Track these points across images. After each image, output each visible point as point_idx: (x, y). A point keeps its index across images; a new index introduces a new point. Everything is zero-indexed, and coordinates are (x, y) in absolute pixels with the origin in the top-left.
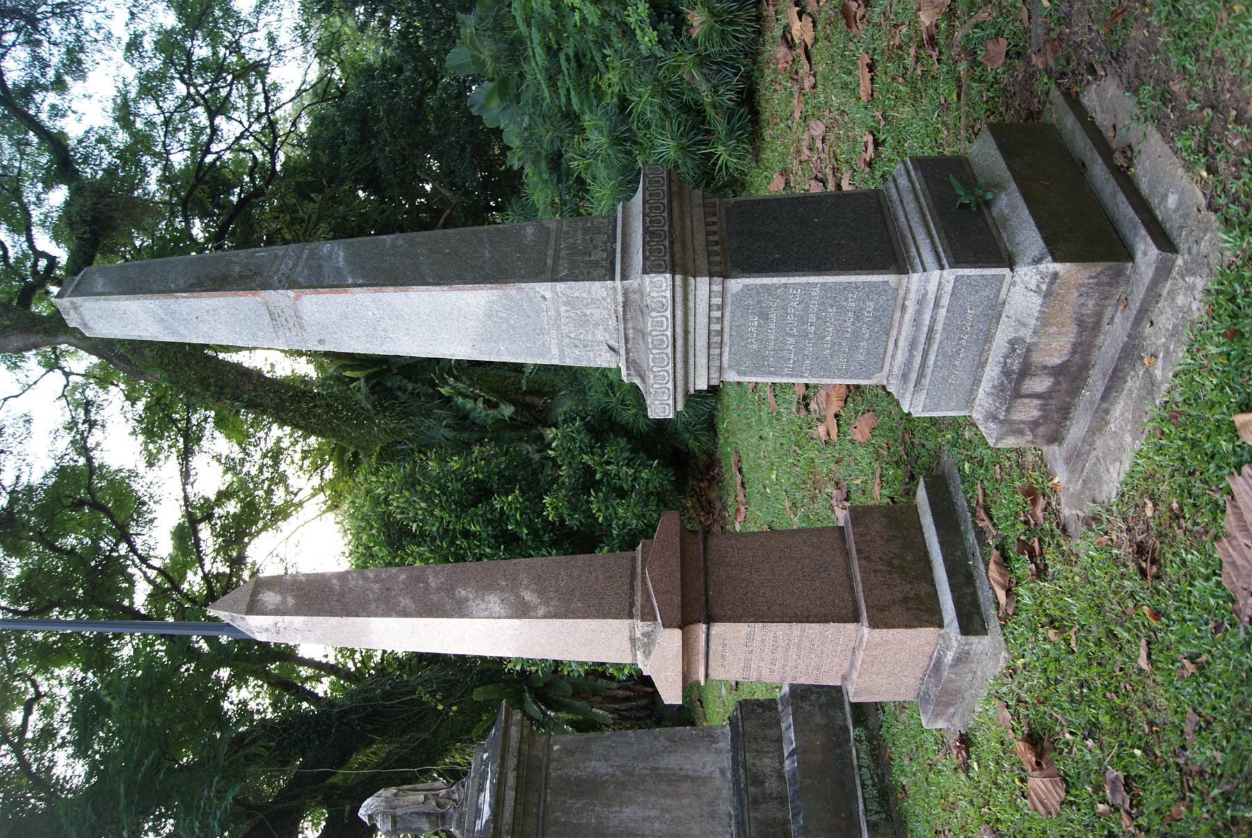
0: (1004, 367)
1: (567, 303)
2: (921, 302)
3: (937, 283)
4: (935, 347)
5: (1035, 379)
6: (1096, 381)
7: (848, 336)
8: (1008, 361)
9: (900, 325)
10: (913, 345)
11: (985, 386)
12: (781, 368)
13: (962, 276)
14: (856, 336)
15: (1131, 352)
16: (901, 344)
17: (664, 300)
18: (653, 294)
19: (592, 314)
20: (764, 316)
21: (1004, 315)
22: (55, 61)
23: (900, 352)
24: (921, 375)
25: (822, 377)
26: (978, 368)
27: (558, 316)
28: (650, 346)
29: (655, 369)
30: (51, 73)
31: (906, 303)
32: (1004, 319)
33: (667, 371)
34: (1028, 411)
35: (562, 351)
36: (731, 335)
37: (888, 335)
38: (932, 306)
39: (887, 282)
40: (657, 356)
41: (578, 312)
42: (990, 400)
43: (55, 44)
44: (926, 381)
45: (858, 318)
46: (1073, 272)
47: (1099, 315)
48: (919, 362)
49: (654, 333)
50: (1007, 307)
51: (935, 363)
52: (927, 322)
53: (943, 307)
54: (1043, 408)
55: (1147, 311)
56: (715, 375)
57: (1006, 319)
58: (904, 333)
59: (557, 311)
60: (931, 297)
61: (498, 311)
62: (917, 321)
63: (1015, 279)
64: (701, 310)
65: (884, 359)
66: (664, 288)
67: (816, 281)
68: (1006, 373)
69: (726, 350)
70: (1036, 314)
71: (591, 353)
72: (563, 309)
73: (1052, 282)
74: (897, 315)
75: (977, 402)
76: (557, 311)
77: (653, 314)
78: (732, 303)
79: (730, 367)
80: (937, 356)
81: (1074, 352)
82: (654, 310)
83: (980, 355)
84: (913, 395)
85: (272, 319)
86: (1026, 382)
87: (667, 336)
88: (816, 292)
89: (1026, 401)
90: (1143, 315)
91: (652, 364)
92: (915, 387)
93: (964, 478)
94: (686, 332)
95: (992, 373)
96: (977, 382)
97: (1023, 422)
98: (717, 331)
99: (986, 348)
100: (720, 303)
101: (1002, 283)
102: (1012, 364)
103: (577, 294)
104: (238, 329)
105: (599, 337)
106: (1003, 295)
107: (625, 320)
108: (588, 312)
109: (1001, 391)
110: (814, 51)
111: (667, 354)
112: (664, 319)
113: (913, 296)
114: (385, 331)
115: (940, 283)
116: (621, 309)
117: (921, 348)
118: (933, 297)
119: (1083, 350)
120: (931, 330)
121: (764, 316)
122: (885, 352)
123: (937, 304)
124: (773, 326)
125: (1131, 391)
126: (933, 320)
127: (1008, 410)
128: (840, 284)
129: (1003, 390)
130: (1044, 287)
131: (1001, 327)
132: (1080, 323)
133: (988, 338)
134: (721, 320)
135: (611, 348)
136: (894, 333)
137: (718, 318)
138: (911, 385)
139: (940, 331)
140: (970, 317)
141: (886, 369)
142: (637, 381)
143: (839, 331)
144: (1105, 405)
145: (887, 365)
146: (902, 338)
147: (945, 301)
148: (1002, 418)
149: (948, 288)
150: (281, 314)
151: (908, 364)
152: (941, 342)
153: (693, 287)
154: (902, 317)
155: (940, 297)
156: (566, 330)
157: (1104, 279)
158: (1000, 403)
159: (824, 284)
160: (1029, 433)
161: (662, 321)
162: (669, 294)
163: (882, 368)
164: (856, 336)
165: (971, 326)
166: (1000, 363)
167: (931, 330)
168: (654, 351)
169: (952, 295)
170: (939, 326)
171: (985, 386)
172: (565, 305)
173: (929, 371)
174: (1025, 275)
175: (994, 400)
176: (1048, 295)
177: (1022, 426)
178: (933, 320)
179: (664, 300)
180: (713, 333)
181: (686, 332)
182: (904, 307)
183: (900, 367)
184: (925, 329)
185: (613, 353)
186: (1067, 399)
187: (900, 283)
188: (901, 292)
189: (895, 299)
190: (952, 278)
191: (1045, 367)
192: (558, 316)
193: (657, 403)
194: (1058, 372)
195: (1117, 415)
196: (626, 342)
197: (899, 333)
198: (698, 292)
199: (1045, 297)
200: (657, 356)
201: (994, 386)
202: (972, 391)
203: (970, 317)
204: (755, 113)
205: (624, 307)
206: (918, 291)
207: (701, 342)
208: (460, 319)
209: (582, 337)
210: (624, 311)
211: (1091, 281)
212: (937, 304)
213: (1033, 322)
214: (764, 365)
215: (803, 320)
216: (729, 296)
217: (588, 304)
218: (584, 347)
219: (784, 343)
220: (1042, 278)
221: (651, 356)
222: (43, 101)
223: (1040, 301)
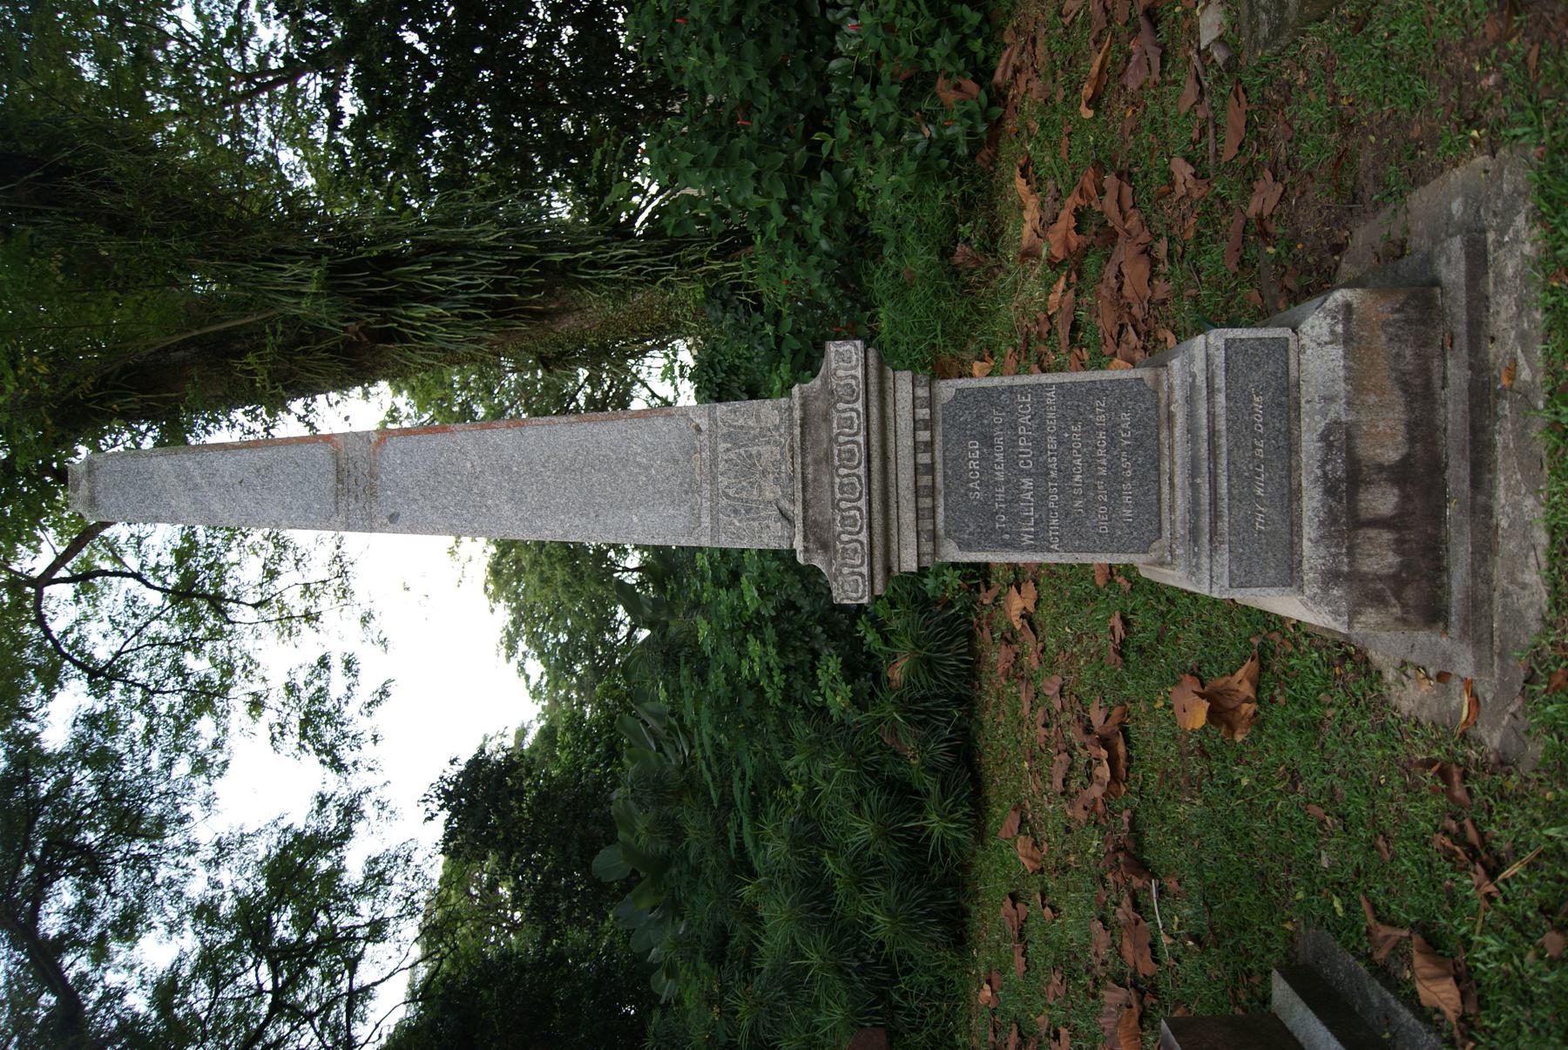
0: (1324, 483)
1: (728, 437)
2: (1190, 400)
3: (1203, 354)
4: (1223, 461)
5: (1373, 489)
6: (1458, 473)
7: (1103, 472)
8: (1328, 467)
9: (1171, 448)
10: (1194, 473)
11: (1309, 531)
12: (1018, 534)
13: (1234, 340)
14: (1115, 476)
15: (1482, 397)
16: (1177, 480)
17: (854, 382)
18: (841, 373)
19: (759, 455)
20: (987, 441)
21: (1303, 401)
22: (107, 915)
23: (1179, 493)
24: (1215, 516)
25: (1077, 550)
26: (1290, 501)
27: (714, 462)
28: (837, 463)
29: (843, 505)
30: (94, 930)
31: (1172, 408)
32: (1305, 407)
33: (859, 509)
34: (1380, 557)
35: (715, 531)
36: (945, 475)
37: (1158, 468)
38: (1204, 393)
39: (1141, 379)
40: (846, 481)
41: (742, 451)
42: (1322, 551)
43: (114, 896)
44: (1224, 525)
45: (1113, 442)
46: (1370, 302)
47: (1425, 371)
48: (1207, 493)
49: (842, 439)
50: (1304, 388)
51: (1230, 492)
52: (1204, 421)
53: (1219, 390)
54: (1400, 546)
55: (1480, 323)
56: (927, 547)
57: (1308, 406)
58: (1178, 460)
59: (714, 450)
60: (1201, 380)
61: (636, 454)
62: (1191, 430)
63: (1302, 342)
64: (903, 426)
65: (1159, 515)
66: (854, 363)
67: (1049, 381)
68: (1330, 491)
69: (941, 501)
70: (1341, 374)
71: (756, 524)
72: (722, 446)
73: (1347, 320)
74: (1164, 434)
75: (1306, 566)
76: (714, 450)
77: (841, 406)
78: (944, 421)
79: (948, 533)
80: (1229, 480)
81: (1412, 440)
82: (840, 399)
83: (1289, 477)
84: (1211, 557)
85: (339, 481)
86: (1362, 496)
87: (857, 443)
88: (1051, 397)
89: (1372, 533)
90: (1478, 331)
91: (838, 496)
92: (1211, 540)
93: (1338, 929)
94: (885, 458)
95: (1312, 501)
96: (1295, 527)
97: (1380, 578)
98: (925, 465)
99: (1294, 464)
100: (927, 417)
101: (1287, 351)
102: (1334, 470)
103: (741, 422)
104: (288, 500)
105: (769, 495)
106: (1293, 373)
107: (803, 449)
108: (754, 450)
109: (1331, 524)
110: (1038, 618)
111: (859, 477)
112: (854, 414)
113: (1178, 395)
114: (482, 495)
115: (1208, 356)
116: (797, 431)
117: (1205, 470)
118: (1204, 378)
119: (1422, 430)
120: (1213, 434)
121: (987, 441)
122: (1159, 500)
123: (1211, 391)
124: (1000, 457)
125: (1506, 447)
126: (1212, 416)
127: (1350, 552)
128: (1081, 384)
129: (1335, 521)
130: (1339, 329)
131: (1305, 421)
132: (1405, 387)
133: (1291, 447)
134: (930, 445)
135: (783, 514)
136: (1166, 465)
137: (926, 443)
138: (1205, 539)
139: (1224, 433)
140: (1258, 408)
141: (1166, 534)
142: (818, 562)
143: (1090, 464)
144: (1481, 499)
145: (1166, 525)
146: (1178, 470)
147: (1220, 382)
148: (1345, 569)
149: (1219, 359)
150: (352, 470)
151: (1194, 510)
152: (1229, 452)
153: (894, 517)
154: (1171, 435)
155: (1213, 378)
156: (723, 481)
157: (1413, 314)
158: (1337, 545)
159: (1060, 386)
160: (1393, 601)
161: (855, 525)
162: (859, 373)
163: (1160, 530)
164: (1115, 476)
165: (1264, 424)
166: (1317, 479)
167: (1213, 434)
168: (843, 471)
169: (1227, 371)
170: (1222, 425)
171: (1309, 531)
172: (725, 441)
173: (1224, 505)
174: (1312, 327)
175: (1327, 547)
176: (1348, 340)
177: (1379, 586)
178: (1212, 416)
179: (854, 382)
180: (921, 469)
181: (885, 458)
182: (1170, 417)
183: (1183, 522)
184: (1204, 433)
185: (785, 523)
186: (1429, 530)
187: (1157, 380)
188: (1163, 396)
189: (1157, 407)
190: (1221, 343)
191: (1381, 468)
192: (714, 462)
193: (846, 570)
194: (1400, 474)
195: (1503, 501)
196: (804, 489)
197: (1172, 463)
198: (898, 395)
199: (1346, 343)
200: (846, 481)
201: (1322, 523)
202: (1292, 545)
203: (1258, 408)
204: (977, 782)
205: (802, 426)
206: (1183, 382)
207: (905, 479)
208: (585, 470)
209: (744, 495)
210: (802, 433)
211: (1396, 316)
212: (1211, 391)
213: (1341, 387)
214: (993, 529)
215: (1039, 446)
216: (939, 407)
217: (755, 437)
218: (748, 511)
219: (1018, 485)
220: (1334, 318)
221: (837, 480)
222: (72, 965)
223: (1341, 352)
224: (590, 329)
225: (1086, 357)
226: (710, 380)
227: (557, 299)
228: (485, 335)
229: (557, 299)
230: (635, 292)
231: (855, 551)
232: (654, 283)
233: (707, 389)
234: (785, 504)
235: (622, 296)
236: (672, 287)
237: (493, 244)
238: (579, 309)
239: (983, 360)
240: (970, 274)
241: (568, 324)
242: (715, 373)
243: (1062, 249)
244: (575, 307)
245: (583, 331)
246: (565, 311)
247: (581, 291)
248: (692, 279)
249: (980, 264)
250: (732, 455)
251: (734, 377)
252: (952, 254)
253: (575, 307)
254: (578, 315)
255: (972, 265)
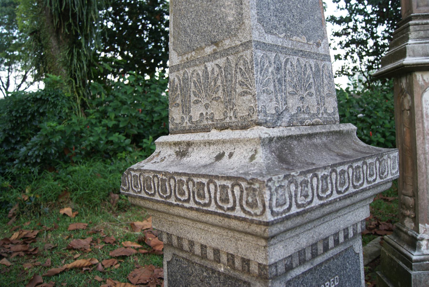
41: (311, 80)
71: (272, 89)
108: (313, 90)
156: (294, 59)
224: (51, 51)
225: (116, 267)
226: (50, 95)
227: (64, 39)
228: (53, 7)
229: (64, 39)
230: (67, 70)
231: (306, 196)
232: (71, 77)
233: (46, 94)
234: (286, 119)
235: (65, 65)
236: (69, 84)
237: (89, 17)
238: (59, 48)
239: (73, 212)
240: (109, 201)
241: (53, 42)
242: (53, 98)
243: (155, 244)
244: (60, 46)
245: (50, 48)
246: (59, 42)
247: (68, 49)
248: (73, 92)
249: (112, 204)
250: (309, 71)
251: (51, 106)
252: (114, 193)
253: (60, 46)
254: (57, 47)
255: (112, 201)
